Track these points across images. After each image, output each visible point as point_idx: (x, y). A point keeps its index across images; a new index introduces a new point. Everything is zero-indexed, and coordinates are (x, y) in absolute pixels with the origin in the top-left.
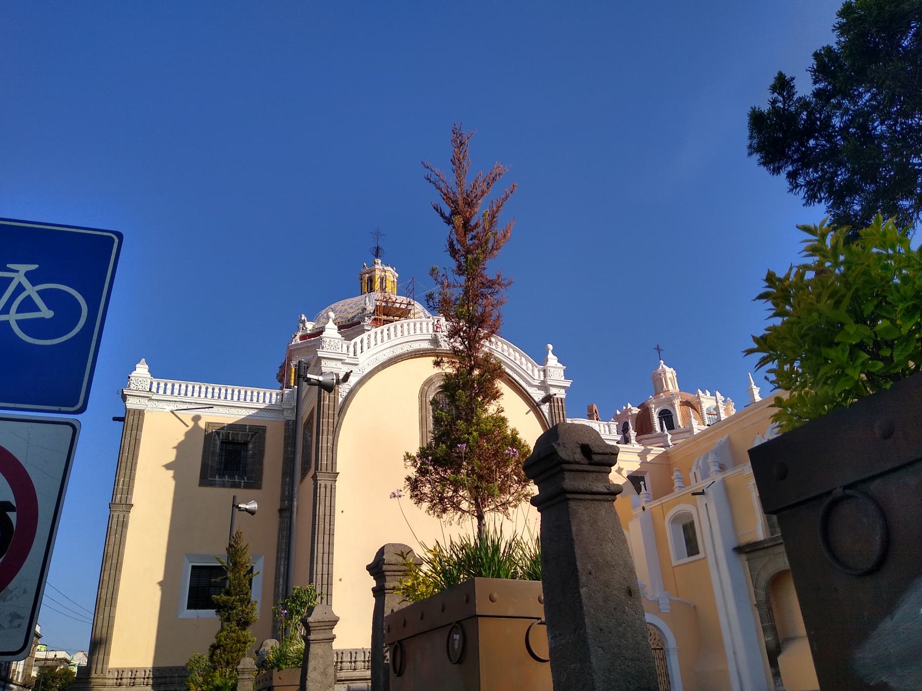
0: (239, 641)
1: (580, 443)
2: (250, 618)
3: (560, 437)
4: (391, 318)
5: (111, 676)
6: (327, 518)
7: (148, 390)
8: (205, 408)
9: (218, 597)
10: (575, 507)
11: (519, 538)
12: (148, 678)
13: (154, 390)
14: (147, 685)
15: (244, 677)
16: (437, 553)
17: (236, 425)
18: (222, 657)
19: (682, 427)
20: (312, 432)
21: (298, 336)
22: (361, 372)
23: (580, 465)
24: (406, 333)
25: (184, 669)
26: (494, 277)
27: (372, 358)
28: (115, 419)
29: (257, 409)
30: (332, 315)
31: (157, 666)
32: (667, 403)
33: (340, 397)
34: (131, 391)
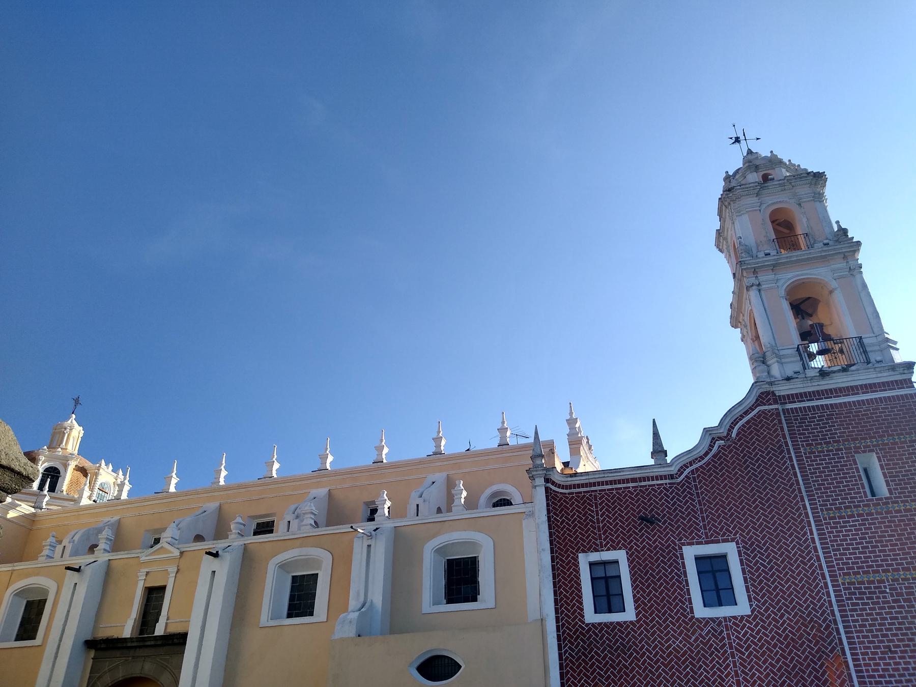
19: (65, 493)
32: (60, 461)
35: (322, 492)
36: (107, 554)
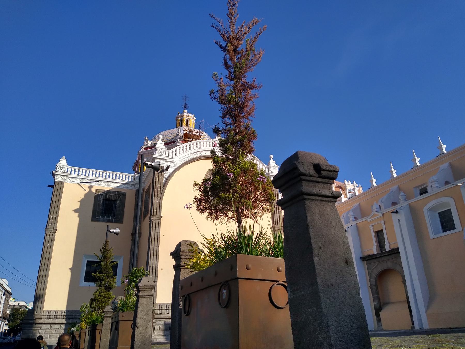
0: (106, 297)
1: (313, 163)
2: (112, 285)
3: (299, 158)
4: (191, 140)
5: (45, 314)
6: (156, 238)
7: (66, 172)
8: (95, 182)
9: (95, 274)
10: (309, 205)
11: (264, 232)
12: (63, 315)
13: (69, 172)
14: (63, 319)
15: (107, 316)
16: (212, 245)
17: (111, 191)
18: (96, 305)
20: (149, 196)
21: (144, 148)
22: (175, 166)
23: (312, 178)
24: (199, 147)
25: (78, 312)
26: (252, 81)
27: (181, 159)
28: (49, 186)
29: (122, 183)
30: (161, 136)
31: (71, 309)
33: (164, 178)
34: (57, 172)
35: (446, 165)
36: (354, 222)
